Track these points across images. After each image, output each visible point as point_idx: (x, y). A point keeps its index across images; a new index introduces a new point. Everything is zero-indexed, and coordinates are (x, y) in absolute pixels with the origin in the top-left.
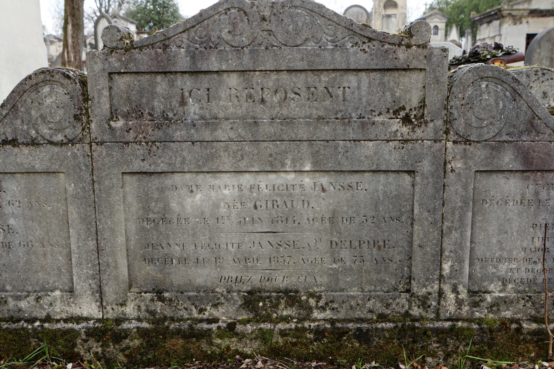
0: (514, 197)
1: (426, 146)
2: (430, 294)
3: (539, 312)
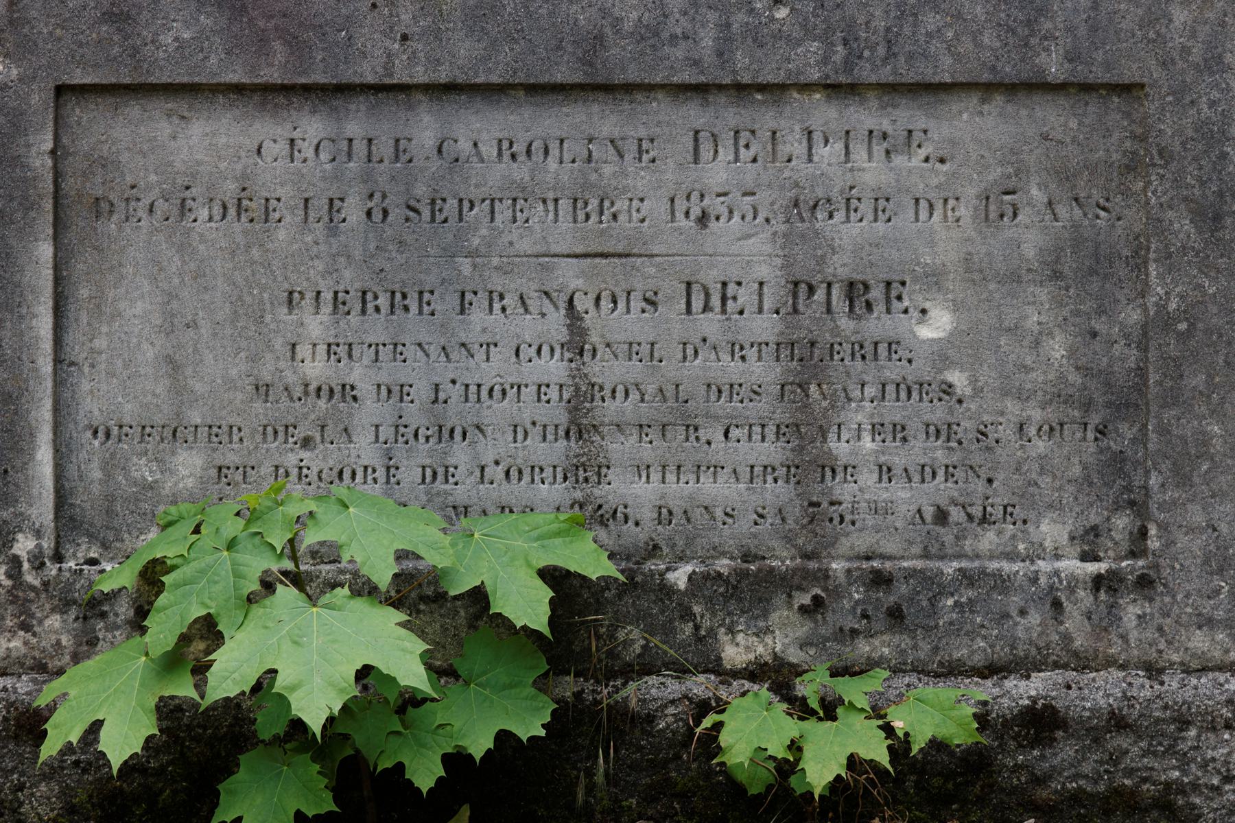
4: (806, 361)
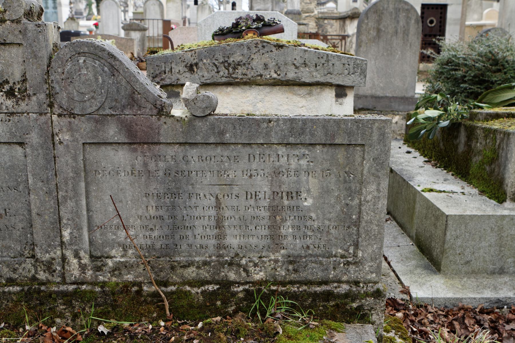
0: (124, 168)
1: (32, 119)
2: (53, 259)
3: (158, 276)
4: (275, 210)
